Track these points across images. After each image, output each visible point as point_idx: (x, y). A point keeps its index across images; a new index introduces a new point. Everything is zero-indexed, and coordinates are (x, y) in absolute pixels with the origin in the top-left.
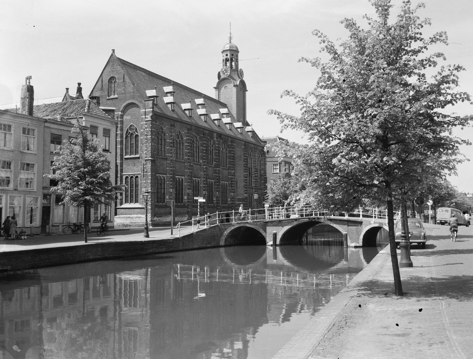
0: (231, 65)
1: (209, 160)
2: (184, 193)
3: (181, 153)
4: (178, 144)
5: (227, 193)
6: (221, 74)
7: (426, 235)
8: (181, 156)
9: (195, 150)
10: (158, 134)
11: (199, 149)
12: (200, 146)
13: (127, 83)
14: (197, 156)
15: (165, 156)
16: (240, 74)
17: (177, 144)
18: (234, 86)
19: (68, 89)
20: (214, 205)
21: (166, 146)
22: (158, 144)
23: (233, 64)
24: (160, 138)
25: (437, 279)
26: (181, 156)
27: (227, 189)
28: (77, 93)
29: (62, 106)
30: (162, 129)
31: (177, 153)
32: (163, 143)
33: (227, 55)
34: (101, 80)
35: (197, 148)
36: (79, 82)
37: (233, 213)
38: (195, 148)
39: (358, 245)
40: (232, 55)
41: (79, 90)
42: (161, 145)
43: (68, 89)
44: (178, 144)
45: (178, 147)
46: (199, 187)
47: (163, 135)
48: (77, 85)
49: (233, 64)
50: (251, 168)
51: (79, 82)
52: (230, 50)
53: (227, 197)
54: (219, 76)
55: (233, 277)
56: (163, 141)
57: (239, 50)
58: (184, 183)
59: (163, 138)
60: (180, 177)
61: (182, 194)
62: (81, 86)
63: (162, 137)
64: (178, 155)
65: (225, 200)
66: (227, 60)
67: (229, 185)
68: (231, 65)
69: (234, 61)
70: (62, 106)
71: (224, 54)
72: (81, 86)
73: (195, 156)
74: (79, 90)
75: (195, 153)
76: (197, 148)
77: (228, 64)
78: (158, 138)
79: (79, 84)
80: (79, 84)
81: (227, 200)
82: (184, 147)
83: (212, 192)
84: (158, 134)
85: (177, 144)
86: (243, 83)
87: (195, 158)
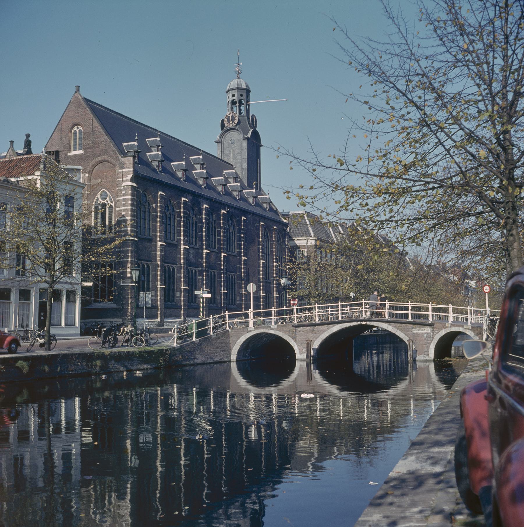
0: (240, 110)
1: (210, 242)
2: (175, 288)
3: (172, 231)
4: (168, 219)
5: (235, 289)
6: (226, 123)
7: (378, 449)
8: (172, 235)
9: (191, 228)
10: (140, 203)
11: (196, 227)
12: (198, 222)
13: (97, 132)
14: (194, 236)
15: (149, 236)
16: (253, 122)
17: (166, 219)
18: (243, 139)
19: (13, 142)
20: (217, 306)
21: (151, 222)
22: (140, 218)
23: (243, 108)
24: (142, 209)
25: (492, 446)
26: (172, 235)
27: (235, 283)
28: (24, 149)
29: (6, 164)
30: (146, 196)
31: (166, 232)
32: (147, 217)
33: (233, 96)
34: (59, 127)
35: (194, 225)
36: (27, 133)
37: (227, 316)
38: (191, 225)
39: (427, 358)
40: (242, 95)
41: (28, 144)
42: (145, 219)
43: (13, 142)
44: (168, 219)
45: (168, 222)
46: (196, 279)
47: (147, 206)
48: (25, 138)
49: (243, 108)
50: (269, 255)
51: (27, 133)
52: (238, 89)
53: (235, 294)
54: (223, 125)
55: (184, 456)
56: (147, 214)
57: (251, 89)
58: (176, 273)
59: (147, 210)
60: (170, 265)
61: (173, 290)
62: (30, 139)
63: (145, 209)
64: (168, 234)
65: (232, 300)
66: (233, 103)
67: (237, 277)
68: (240, 110)
69: (243, 104)
70: (6, 164)
71: (230, 95)
72: (30, 139)
73: (191, 236)
74: (28, 144)
75: (191, 232)
76: (194, 225)
77: (236, 108)
78: (140, 210)
79: (28, 136)
80: (28, 136)
81: (235, 300)
82: (176, 223)
83: (215, 287)
84: (140, 203)
85: (166, 219)
86: (256, 134)
87: (191, 238)
